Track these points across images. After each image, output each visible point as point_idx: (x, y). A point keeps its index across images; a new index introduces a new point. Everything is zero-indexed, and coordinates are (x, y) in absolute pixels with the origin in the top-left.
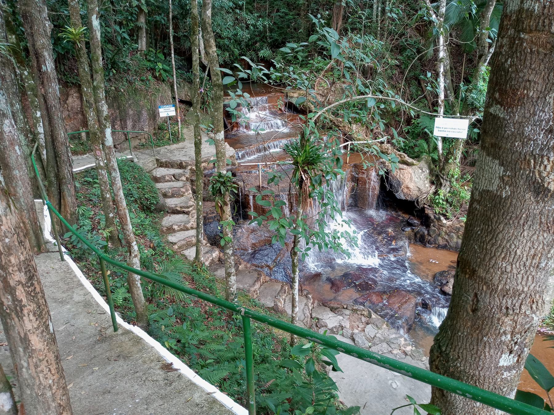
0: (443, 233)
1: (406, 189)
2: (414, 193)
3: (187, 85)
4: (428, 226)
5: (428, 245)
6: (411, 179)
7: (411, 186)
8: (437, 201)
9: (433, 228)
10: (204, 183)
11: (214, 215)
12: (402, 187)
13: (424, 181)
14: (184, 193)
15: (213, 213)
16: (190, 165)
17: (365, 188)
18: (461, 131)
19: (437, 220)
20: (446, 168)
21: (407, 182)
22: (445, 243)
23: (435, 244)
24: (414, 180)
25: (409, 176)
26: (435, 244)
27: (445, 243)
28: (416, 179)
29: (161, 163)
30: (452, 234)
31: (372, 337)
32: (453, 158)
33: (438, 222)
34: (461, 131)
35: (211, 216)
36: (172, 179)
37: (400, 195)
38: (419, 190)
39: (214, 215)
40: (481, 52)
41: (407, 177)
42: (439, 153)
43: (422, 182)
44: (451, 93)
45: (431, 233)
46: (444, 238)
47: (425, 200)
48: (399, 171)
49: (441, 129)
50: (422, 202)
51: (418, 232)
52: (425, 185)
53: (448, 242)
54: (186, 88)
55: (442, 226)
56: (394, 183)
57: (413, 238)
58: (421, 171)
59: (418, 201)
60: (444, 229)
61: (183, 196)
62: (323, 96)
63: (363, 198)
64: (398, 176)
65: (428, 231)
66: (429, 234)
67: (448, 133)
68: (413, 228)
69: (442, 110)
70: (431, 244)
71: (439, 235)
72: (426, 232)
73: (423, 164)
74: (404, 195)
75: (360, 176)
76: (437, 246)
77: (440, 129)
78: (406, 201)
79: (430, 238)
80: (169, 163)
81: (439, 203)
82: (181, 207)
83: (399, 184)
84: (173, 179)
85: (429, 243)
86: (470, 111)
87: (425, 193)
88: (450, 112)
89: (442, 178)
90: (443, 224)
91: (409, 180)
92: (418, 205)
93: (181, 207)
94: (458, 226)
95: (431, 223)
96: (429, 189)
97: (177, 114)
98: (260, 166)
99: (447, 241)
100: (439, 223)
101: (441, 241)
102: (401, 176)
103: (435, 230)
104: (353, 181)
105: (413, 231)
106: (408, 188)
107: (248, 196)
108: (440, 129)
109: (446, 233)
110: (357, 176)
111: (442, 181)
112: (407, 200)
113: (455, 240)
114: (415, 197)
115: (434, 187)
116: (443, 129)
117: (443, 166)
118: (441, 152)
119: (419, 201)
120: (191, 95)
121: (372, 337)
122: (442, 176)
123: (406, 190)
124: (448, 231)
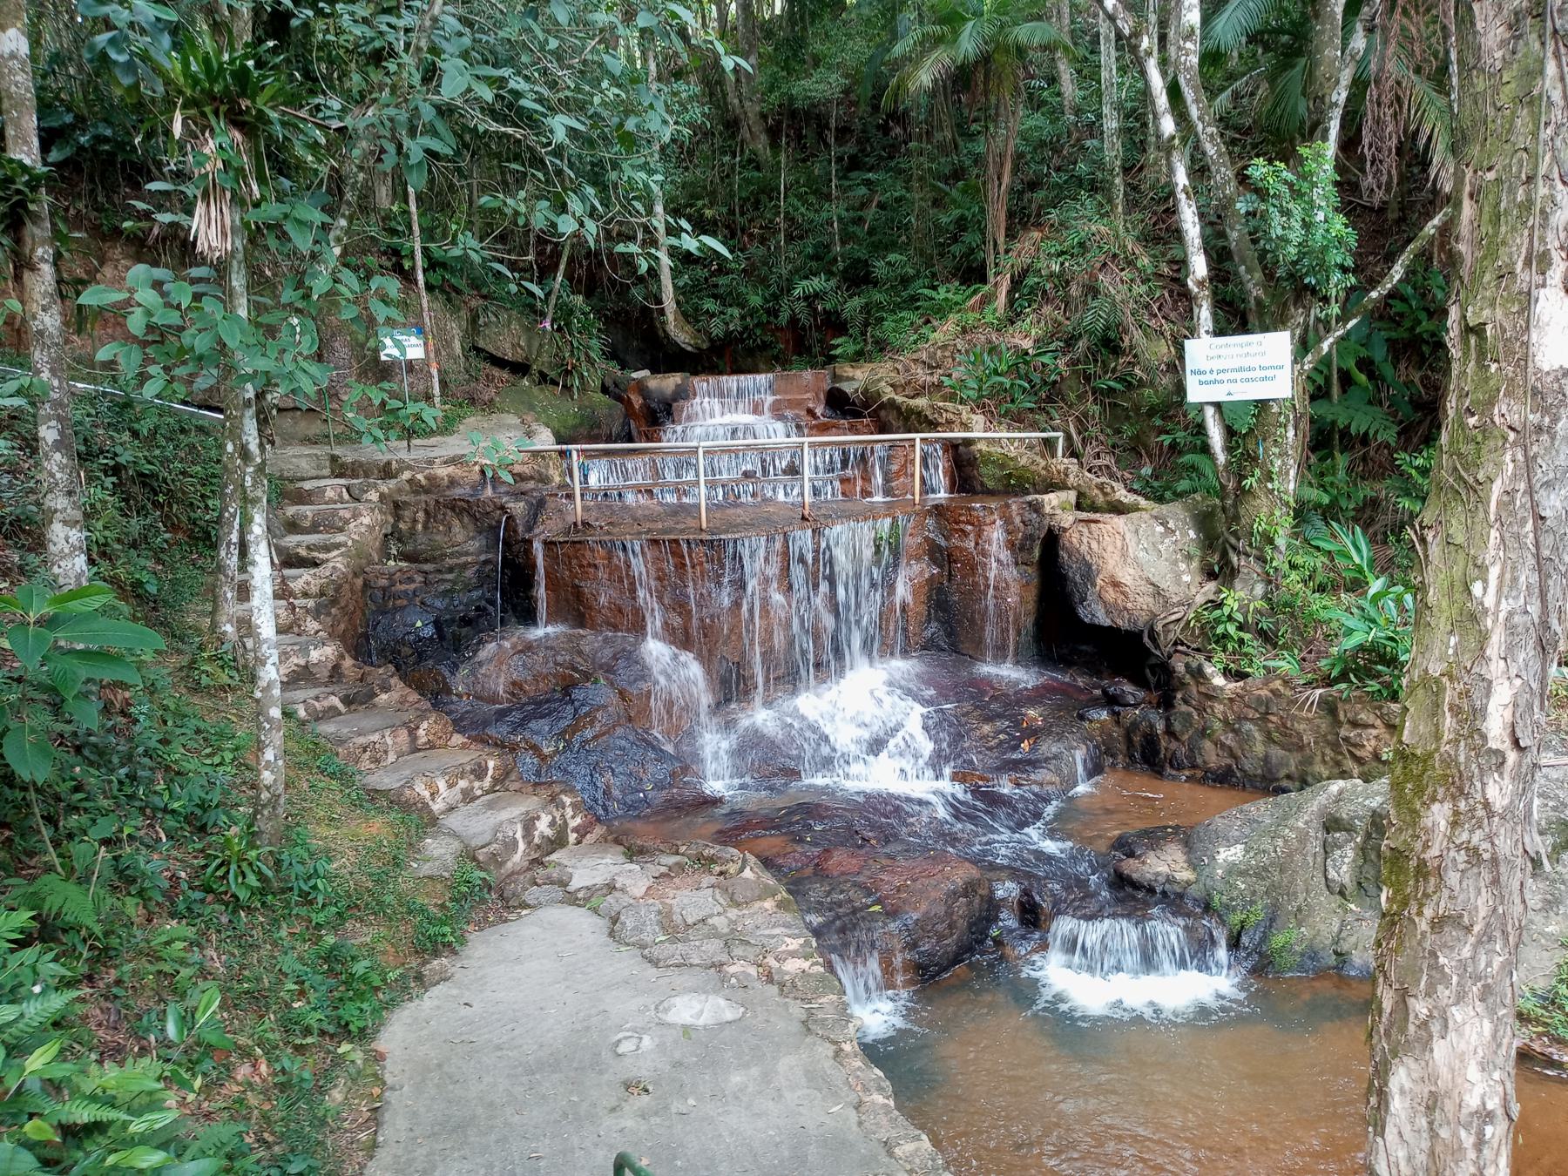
0: (1217, 725)
1: (1110, 590)
2: (1141, 604)
3: (519, 320)
4: (1167, 703)
5: (1169, 770)
6: (1124, 555)
7: (1127, 576)
8: (1220, 630)
9: (1184, 708)
10: (427, 512)
11: (413, 586)
12: (1099, 582)
13: (1175, 563)
14: (347, 522)
15: (411, 580)
16: (409, 467)
17: (975, 584)
18: (1269, 373)
19: (1193, 676)
20: (1242, 512)
21: (1111, 563)
22: (1229, 761)
23: (1194, 767)
24: (1139, 559)
25: (1119, 544)
26: (1194, 767)
27: (1229, 761)
28: (1142, 554)
29: (342, 465)
30: (1248, 726)
31: (690, 921)
32: (1257, 472)
33: (1198, 683)
34: (1269, 373)
35: (403, 587)
36: (341, 496)
37: (1096, 613)
38: (1158, 592)
39: (413, 586)
40: (1314, 117)
41: (1110, 549)
42: (1215, 465)
43: (1163, 566)
44: (1248, 271)
45: (1177, 726)
46: (1223, 745)
47: (1178, 628)
48: (1085, 530)
49: (1208, 377)
50: (1171, 636)
51: (1135, 725)
52: (1178, 576)
53: (1235, 758)
54: (514, 326)
55: (1210, 697)
56: (1074, 573)
57: (1123, 747)
58: (1160, 529)
59: (1152, 631)
60: (1219, 708)
61: (341, 530)
62: (931, 367)
63: (972, 621)
64: (1084, 549)
65: (1168, 719)
66: (1170, 732)
67: (1232, 387)
68: (1117, 708)
69: (1204, 315)
70: (1180, 768)
71: (1203, 733)
72: (1160, 727)
73: (1176, 513)
74: (1108, 613)
75: (955, 541)
76: (1199, 774)
77: (1203, 378)
78: (1113, 631)
79: (1174, 745)
80: (361, 465)
81: (1225, 636)
82: (308, 548)
83: (1089, 573)
84: (346, 496)
85: (1172, 766)
86: (1291, 303)
87: (1180, 604)
88: (1236, 318)
89: (1234, 548)
90: (1215, 688)
91: (1116, 557)
92: (1157, 647)
93: (308, 548)
94: (1265, 693)
95: (1175, 690)
96: (1194, 590)
97: (427, 352)
98: (575, 455)
99: (1232, 755)
100: (1202, 689)
101: (1211, 756)
102: (1094, 545)
103: (1190, 715)
104: (934, 560)
105: (1118, 723)
106: (1116, 585)
107: (530, 542)
108: (1203, 378)
109: (1226, 722)
110: (943, 543)
111: (1235, 559)
112: (1118, 629)
113: (1259, 749)
114: (1143, 618)
115: (1211, 586)
116: (1212, 377)
117: (1235, 506)
118: (1221, 458)
119: (1159, 627)
120: (530, 346)
121: (690, 921)
122: (1233, 540)
123: (1110, 595)
124: (1231, 717)
